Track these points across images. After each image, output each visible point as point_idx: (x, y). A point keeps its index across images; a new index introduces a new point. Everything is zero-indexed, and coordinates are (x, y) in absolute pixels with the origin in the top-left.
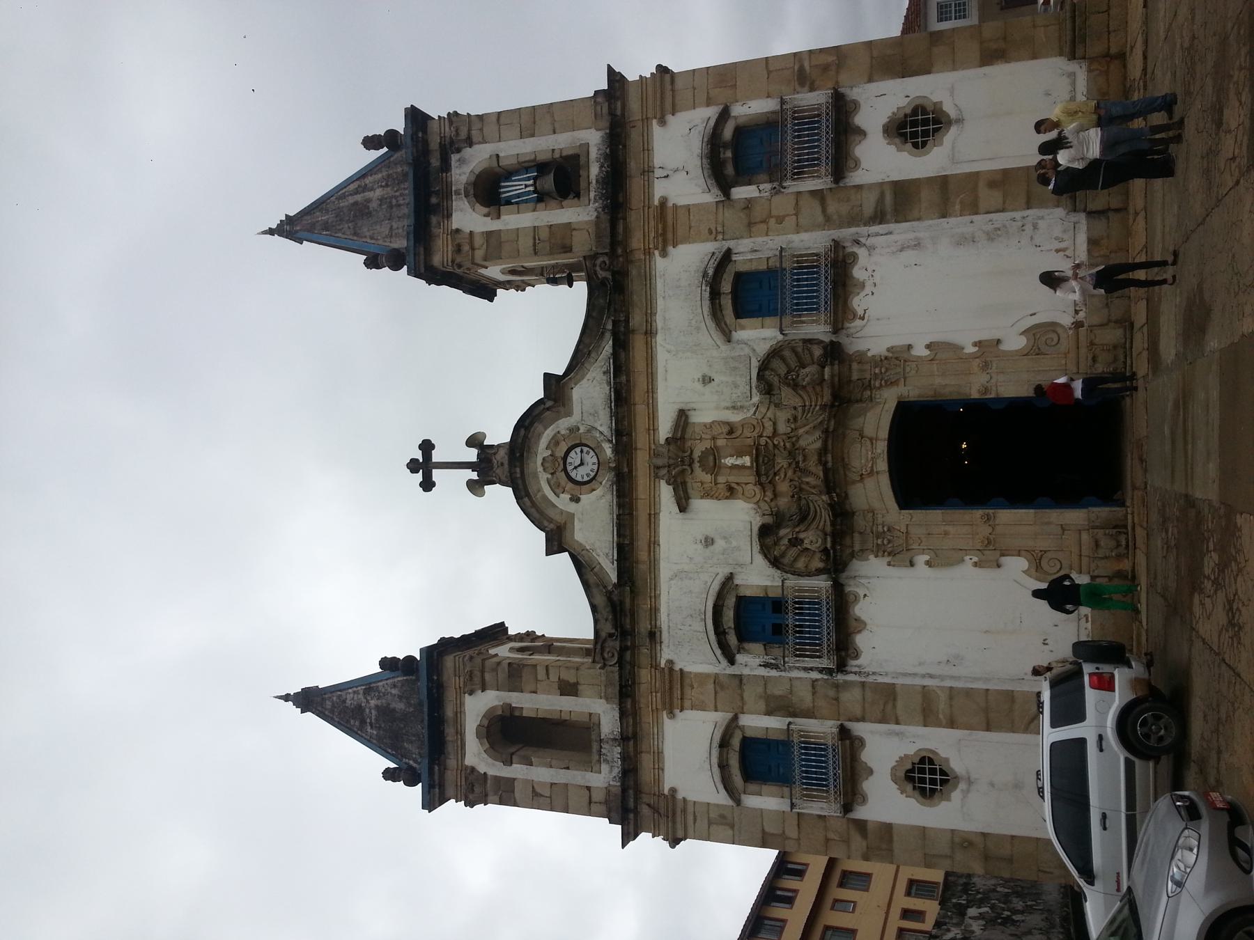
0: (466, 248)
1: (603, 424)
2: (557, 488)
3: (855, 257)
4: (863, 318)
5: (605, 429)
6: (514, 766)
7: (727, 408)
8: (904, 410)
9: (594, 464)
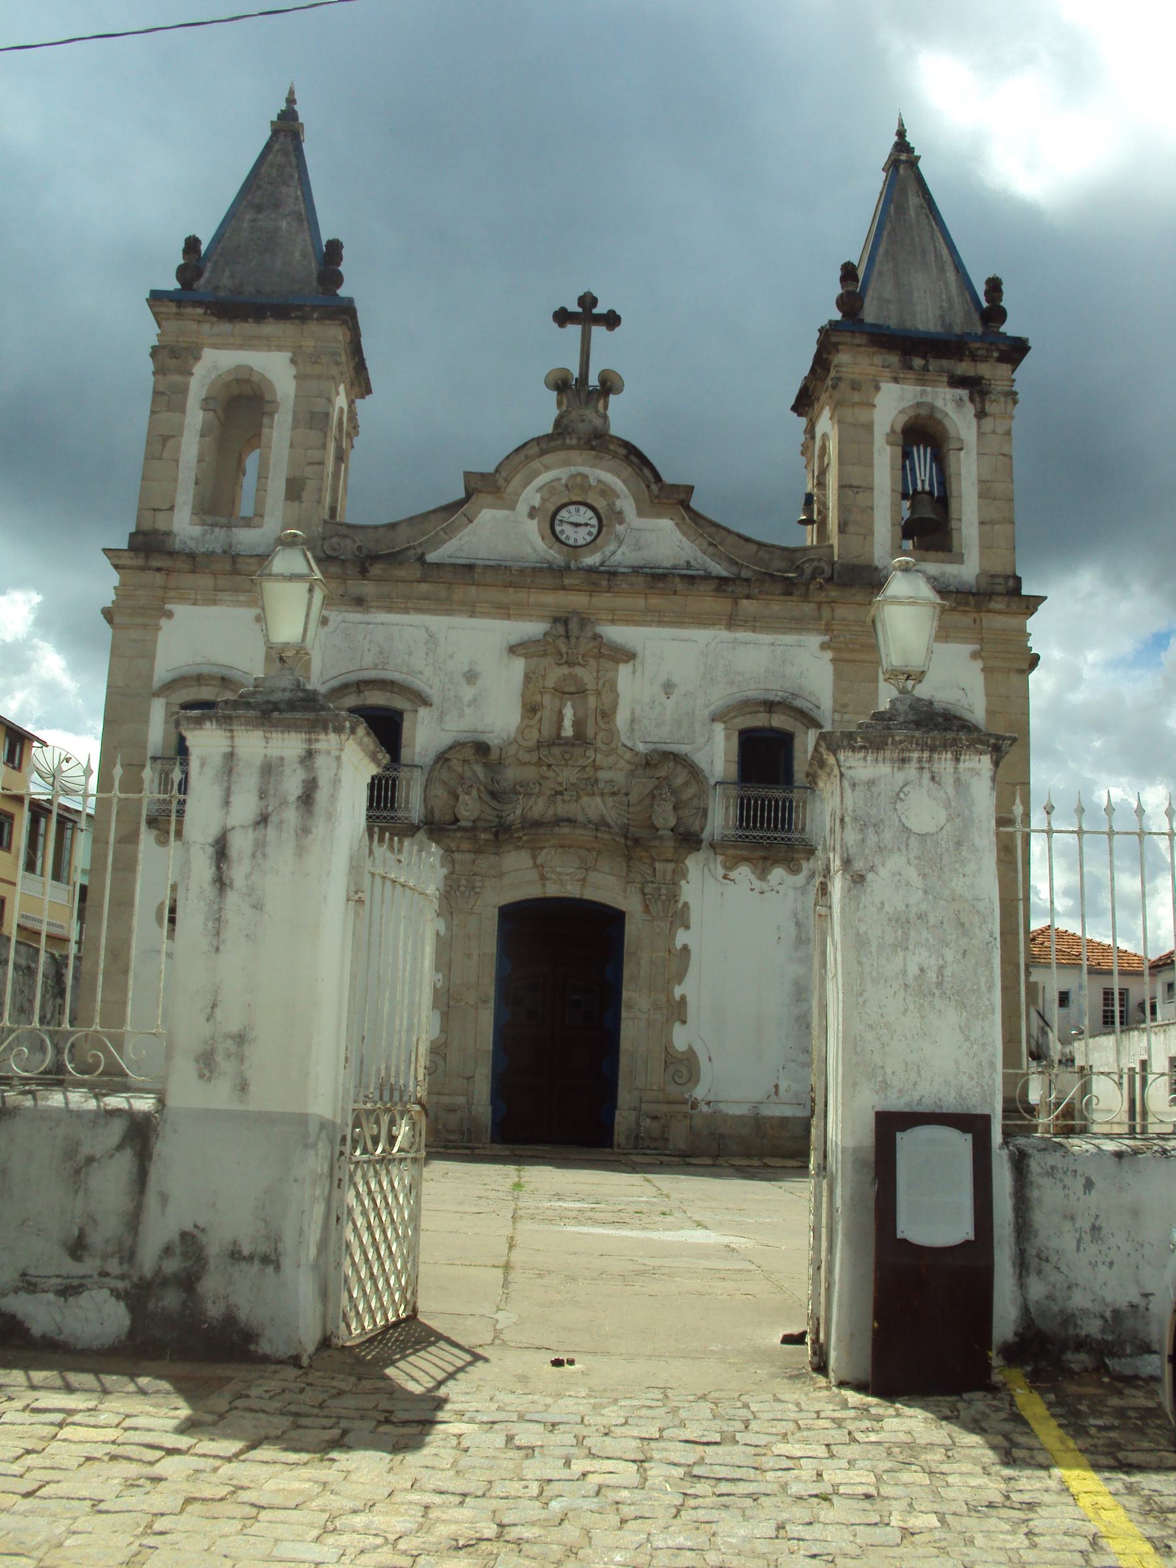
0: (856, 397)
1: (623, 555)
2: (549, 489)
3: (795, 871)
4: (725, 877)
5: (618, 557)
6: (201, 413)
7: (633, 713)
8: (616, 918)
9: (576, 540)
